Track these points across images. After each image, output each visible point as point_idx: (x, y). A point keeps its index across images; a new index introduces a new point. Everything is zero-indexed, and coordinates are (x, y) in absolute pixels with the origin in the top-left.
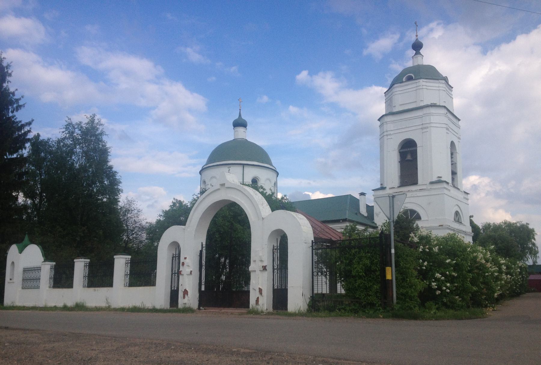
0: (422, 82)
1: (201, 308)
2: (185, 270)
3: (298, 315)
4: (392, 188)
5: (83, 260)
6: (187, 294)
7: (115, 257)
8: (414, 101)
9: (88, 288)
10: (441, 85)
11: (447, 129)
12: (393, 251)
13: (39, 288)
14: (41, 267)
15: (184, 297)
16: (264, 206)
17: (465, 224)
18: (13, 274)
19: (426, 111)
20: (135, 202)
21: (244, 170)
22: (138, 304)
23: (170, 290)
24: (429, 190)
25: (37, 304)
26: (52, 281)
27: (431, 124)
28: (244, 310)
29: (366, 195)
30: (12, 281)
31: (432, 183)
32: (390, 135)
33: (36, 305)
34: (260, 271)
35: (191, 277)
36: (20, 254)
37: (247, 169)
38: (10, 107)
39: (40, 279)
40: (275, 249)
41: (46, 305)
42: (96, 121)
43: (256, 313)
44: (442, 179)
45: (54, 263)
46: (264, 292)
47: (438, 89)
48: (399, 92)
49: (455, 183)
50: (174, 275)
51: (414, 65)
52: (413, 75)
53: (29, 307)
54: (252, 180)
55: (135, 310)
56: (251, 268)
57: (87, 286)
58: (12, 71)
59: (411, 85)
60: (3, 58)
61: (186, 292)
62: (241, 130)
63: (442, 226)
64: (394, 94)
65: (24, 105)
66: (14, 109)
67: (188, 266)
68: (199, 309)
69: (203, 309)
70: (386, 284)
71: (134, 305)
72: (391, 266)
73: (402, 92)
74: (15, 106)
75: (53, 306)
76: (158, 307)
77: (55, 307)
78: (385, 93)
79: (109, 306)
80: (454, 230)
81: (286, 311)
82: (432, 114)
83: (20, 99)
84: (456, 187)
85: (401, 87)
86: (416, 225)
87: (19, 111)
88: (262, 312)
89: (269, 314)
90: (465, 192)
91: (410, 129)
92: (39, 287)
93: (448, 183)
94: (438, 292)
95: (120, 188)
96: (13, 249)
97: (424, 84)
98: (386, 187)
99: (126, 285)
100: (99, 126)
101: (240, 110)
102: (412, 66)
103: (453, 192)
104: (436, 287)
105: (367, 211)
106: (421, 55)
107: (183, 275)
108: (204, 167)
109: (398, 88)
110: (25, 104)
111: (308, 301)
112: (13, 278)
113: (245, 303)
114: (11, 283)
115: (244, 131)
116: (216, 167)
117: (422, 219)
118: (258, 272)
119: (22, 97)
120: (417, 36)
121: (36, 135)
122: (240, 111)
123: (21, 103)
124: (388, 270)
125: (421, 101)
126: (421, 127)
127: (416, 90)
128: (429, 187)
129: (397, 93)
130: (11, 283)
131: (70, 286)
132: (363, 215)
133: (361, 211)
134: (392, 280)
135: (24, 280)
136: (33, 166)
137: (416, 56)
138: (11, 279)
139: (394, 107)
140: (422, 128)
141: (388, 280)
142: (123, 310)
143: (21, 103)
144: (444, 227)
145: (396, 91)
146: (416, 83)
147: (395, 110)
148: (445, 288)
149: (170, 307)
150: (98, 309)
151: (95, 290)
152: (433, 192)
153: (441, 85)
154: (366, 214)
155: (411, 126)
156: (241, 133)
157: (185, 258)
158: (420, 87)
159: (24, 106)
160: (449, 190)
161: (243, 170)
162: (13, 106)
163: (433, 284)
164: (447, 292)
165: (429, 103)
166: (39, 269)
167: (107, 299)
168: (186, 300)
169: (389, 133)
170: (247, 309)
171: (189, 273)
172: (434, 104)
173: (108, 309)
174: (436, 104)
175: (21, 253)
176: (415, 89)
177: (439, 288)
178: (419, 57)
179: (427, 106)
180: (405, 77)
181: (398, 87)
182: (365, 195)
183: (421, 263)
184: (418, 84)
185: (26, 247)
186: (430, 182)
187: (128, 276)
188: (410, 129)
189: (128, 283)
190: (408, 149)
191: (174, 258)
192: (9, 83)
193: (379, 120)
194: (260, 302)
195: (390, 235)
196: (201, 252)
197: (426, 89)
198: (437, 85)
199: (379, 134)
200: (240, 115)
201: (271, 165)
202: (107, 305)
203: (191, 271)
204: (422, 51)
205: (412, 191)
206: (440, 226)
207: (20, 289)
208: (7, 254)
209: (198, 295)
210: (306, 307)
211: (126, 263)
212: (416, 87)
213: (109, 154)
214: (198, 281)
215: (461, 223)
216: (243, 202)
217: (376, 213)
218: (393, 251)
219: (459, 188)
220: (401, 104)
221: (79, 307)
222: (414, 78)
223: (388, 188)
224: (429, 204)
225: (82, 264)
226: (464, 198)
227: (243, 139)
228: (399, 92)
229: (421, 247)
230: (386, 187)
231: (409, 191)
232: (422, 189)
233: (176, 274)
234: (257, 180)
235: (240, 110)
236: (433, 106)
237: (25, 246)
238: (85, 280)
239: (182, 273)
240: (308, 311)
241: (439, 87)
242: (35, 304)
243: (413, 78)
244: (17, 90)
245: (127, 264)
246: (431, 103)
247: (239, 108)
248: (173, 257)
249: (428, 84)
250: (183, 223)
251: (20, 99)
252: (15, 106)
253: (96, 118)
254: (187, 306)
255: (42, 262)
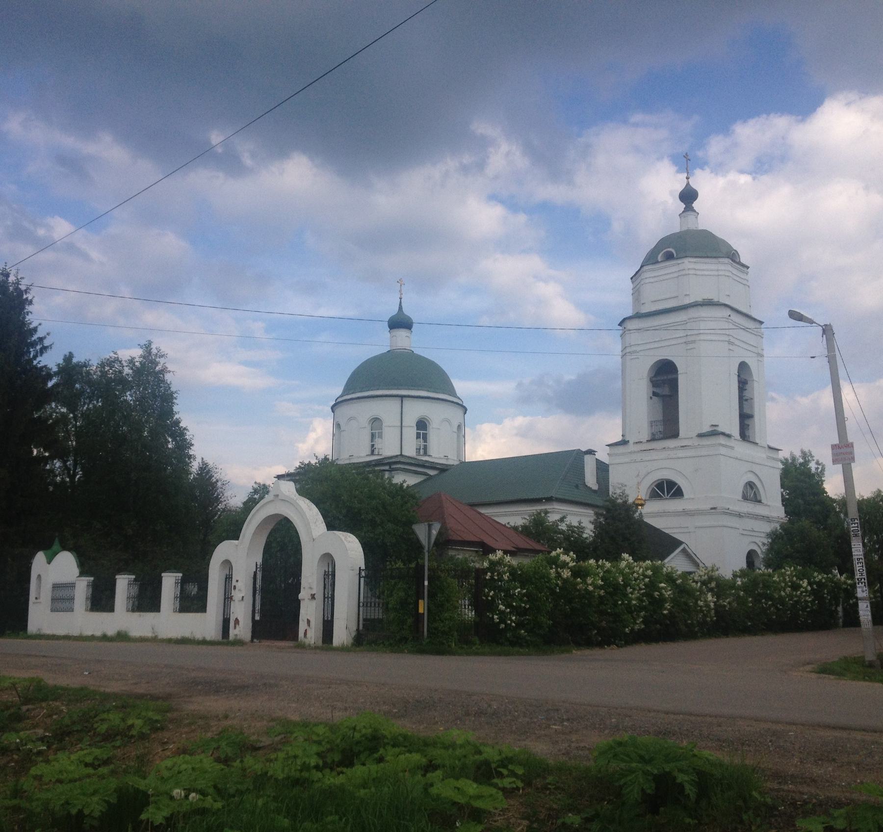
0: (688, 263)
1: (255, 640)
2: (237, 595)
3: (343, 649)
4: (639, 442)
5: (126, 576)
6: (239, 624)
7: (163, 574)
8: (673, 295)
9: (133, 613)
10: (722, 267)
11: (730, 342)
12: (426, 583)
13: (73, 611)
14: (75, 583)
15: (235, 628)
16: (317, 523)
17: (769, 503)
18: (39, 593)
19: (692, 313)
20: (217, 470)
21: (403, 404)
22: (187, 635)
23: (222, 618)
24: (695, 447)
25: (70, 632)
26: (89, 602)
27: (701, 335)
28: (290, 644)
29: (596, 453)
30: (38, 601)
31: (700, 436)
32: (635, 352)
33: (69, 633)
34: (309, 599)
35: (243, 603)
36: (48, 565)
37: (407, 403)
38: (31, 350)
39: (74, 599)
40: (327, 575)
41: (81, 634)
42: (154, 351)
43: (302, 647)
44: (720, 429)
45: (92, 579)
46: (313, 623)
47: (716, 273)
48: (652, 280)
49: (749, 433)
50: (227, 600)
51: (681, 230)
52: (673, 251)
53: (60, 636)
54: (417, 423)
55: (183, 641)
56: (300, 596)
57: (132, 610)
58: (34, 297)
59: (671, 268)
60: (21, 279)
61: (237, 621)
62: (402, 333)
63: (714, 508)
64: (642, 283)
65: (50, 346)
66: (37, 352)
67: (240, 590)
68: (252, 641)
69: (258, 641)
70: (418, 617)
71: (183, 635)
72: (424, 599)
73: (656, 279)
74: (38, 347)
75: (90, 635)
76: (208, 638)
77: (93, 636)
78: (632, 278)
79: (156, 637)
80: (739, 515)
81: (331, 645)
82: (702, 319)
83: (45, 337)
84: (751, 442)
85: (653, 270)
86: (639, 515)
87: (45, 355)
88: (309, 645)
89: (316, 648)
90: (770, 448)
91: (667, 343)
92: (73, 609)
93: (729, 436)
94: (502, 626)
95: (191, 452)
96: (40, 558)
97: (692, 266)
98: (628, 441)
99: (175, 610)
100: (160, 358)
101: (401, 299)
102: (678, 231)
103: (742, 449)
104: (498, 620)
105: (598, 482)
106: (695, 211)
107: (234, 600)
108: (337, 401)
109: (650, 274)
110: (53, 344)
111: (354, 634)
112: (40, 596)
113: (295, 637)
114: (37, 603)
115: (406, 336)
116: (355, 401)
117: (686, 496)
118: (306, 600)
119: (48, 334)
121: (68, 354)
122: (401, 301)
123: (46, 343)
124: (421, 602)
125: (686, 295)
126: (683, 340)
127: (677, 277)
128: (697, 442)
129: (647, 281)
130: (37, 603)
131: (111, 609)
132: (590, 488)
133: (586, 480)
134: (423, 614)
135: (54, 600)
136: (63, 406)
137: (684, 214)
138: (36, 598)
139: (643, 304)
140: (685, 342)
141: (420, 613)
142: (170, 641)
143: (46, 343)
144: (718, 511)
145: (646, 278)
146: (679, 264)
147: (645, 310)
148: (509, 622)
149: (223, 639)
150: (142, 640)
151: (140, 616)
152: (704, 452)
153: (724, 266)
154: (595, 487)
155: (670, 337)
156: (403, 340)
157: (237, 581)
159: (51, 348)
160: (732, 448)
161: (402, 407)
162: (35, 348)
163: (496, 617)
164: (513, 626)
165: (699, 299)
166: (73, 587)
167: (153, 629)
168: (237, 631)
169: (634, 348)
170: (294, 642)
171: (241, 598)
172: (709, 299)
173: (155, 640)
174: (712, 299)
175: (49, 564)
176: (676, 275)
177: (502, 621)
178: (690, 216)
179: (695, 305)
180: (662, 253)
181: (650, 270)
182: (595, 455)
183: (487, 592)
184: (681, 267)
185: (55, 556)
186: (699, 434)
187: (178, 599)
188: (667, 343)
189: (178, 608)
190: (665, 377)
191: (228, 579)
192: (40, 363)
193: (620, 325)
194: (308, 635)
195: (424, 566)
196: (255, 573)
197: (695, 276)
198: (713, 267)
199: (620, 350)
200: (400, 308)
201: (455, 395)
202: (154, 635)
203: (243, 597)
204: (696, 205)
205: (668, 448)
206: (712, 509)
207: (49, 611)
208: (32, 563)
209: (251, 625)
210: (351, 641)
211: (176, 583)
212: (679, 271)
213: (175, 401)
214: (251, 609)
215: (760, 501)
216: (295, 518)
217: (613, 485)
218: (426, 583)
219: (757, 442)
221: (122, 637)
222: (675, 256)
223: (631, 442)
224: (696, 470)
225: (126, 582)
226: (769, 458)
227: (405, 349)
228: (652, 280)
229: (489, 574)
230: (628, 441)
231: (664, 448)
232: (685, 446)
233: (228, 599)
234: (425, 421)
235: (401, 299)
236: (709, 303)
237: (56, 554)
238: (129, 601)
239: (233, 599)
240: (353, 645)
241: (718, 270)
242: (67, 632)
243: (674, 256)
244: (40, 324)
245: (177, 584)
246: (704, 299)
247: (399, 296)
248: (226, 578)
249: (698, 266)
250: (237, 538)
251: (45, 337)
252: (38, 347)
253: (153, 346)
254: (238, 637)
255: (77, 577)
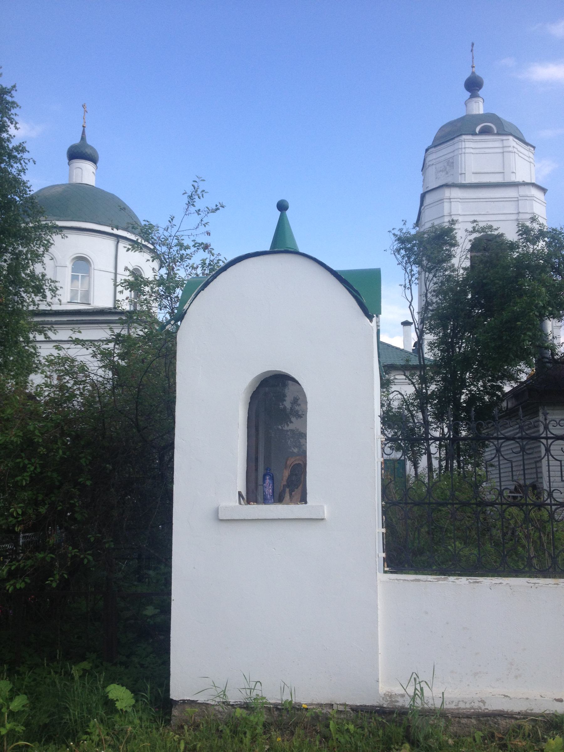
19: (523, 191)
48: (472, 151)
120: (473, 67)
158: (511, 149)
179: (525, 184)
181: (469, 141)
200: (83, 138)
220: (475, 171)
228: (472, 151)
